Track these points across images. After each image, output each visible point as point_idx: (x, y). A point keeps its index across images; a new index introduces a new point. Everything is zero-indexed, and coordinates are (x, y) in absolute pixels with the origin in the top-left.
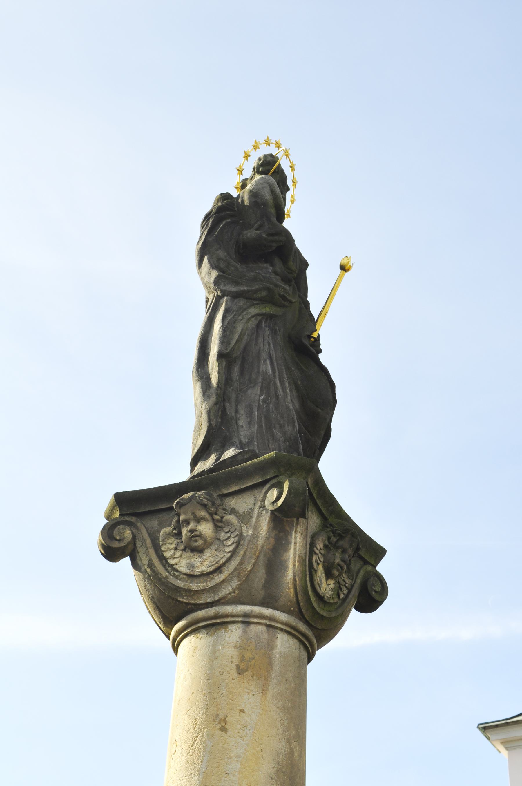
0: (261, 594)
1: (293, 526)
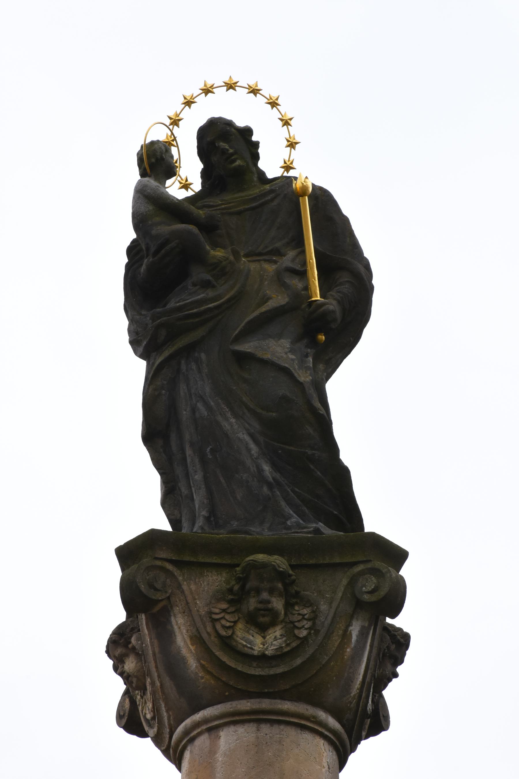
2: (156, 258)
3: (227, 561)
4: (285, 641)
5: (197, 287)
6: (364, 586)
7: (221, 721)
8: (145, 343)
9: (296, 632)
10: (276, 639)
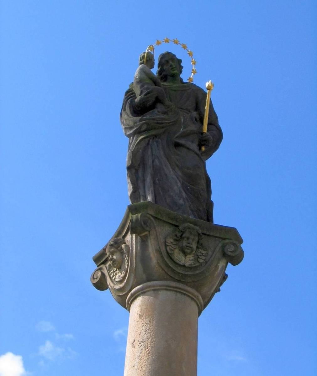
0: (144, 277)
1: (148, 238)
2: (145, 97)
3: (174, 223)
4: (194, 262)
5: (160, 113)
6: (229, 248)
7: (161, 288)
8: (135, 129)
9: (199, 259)
10: (190, 260)
